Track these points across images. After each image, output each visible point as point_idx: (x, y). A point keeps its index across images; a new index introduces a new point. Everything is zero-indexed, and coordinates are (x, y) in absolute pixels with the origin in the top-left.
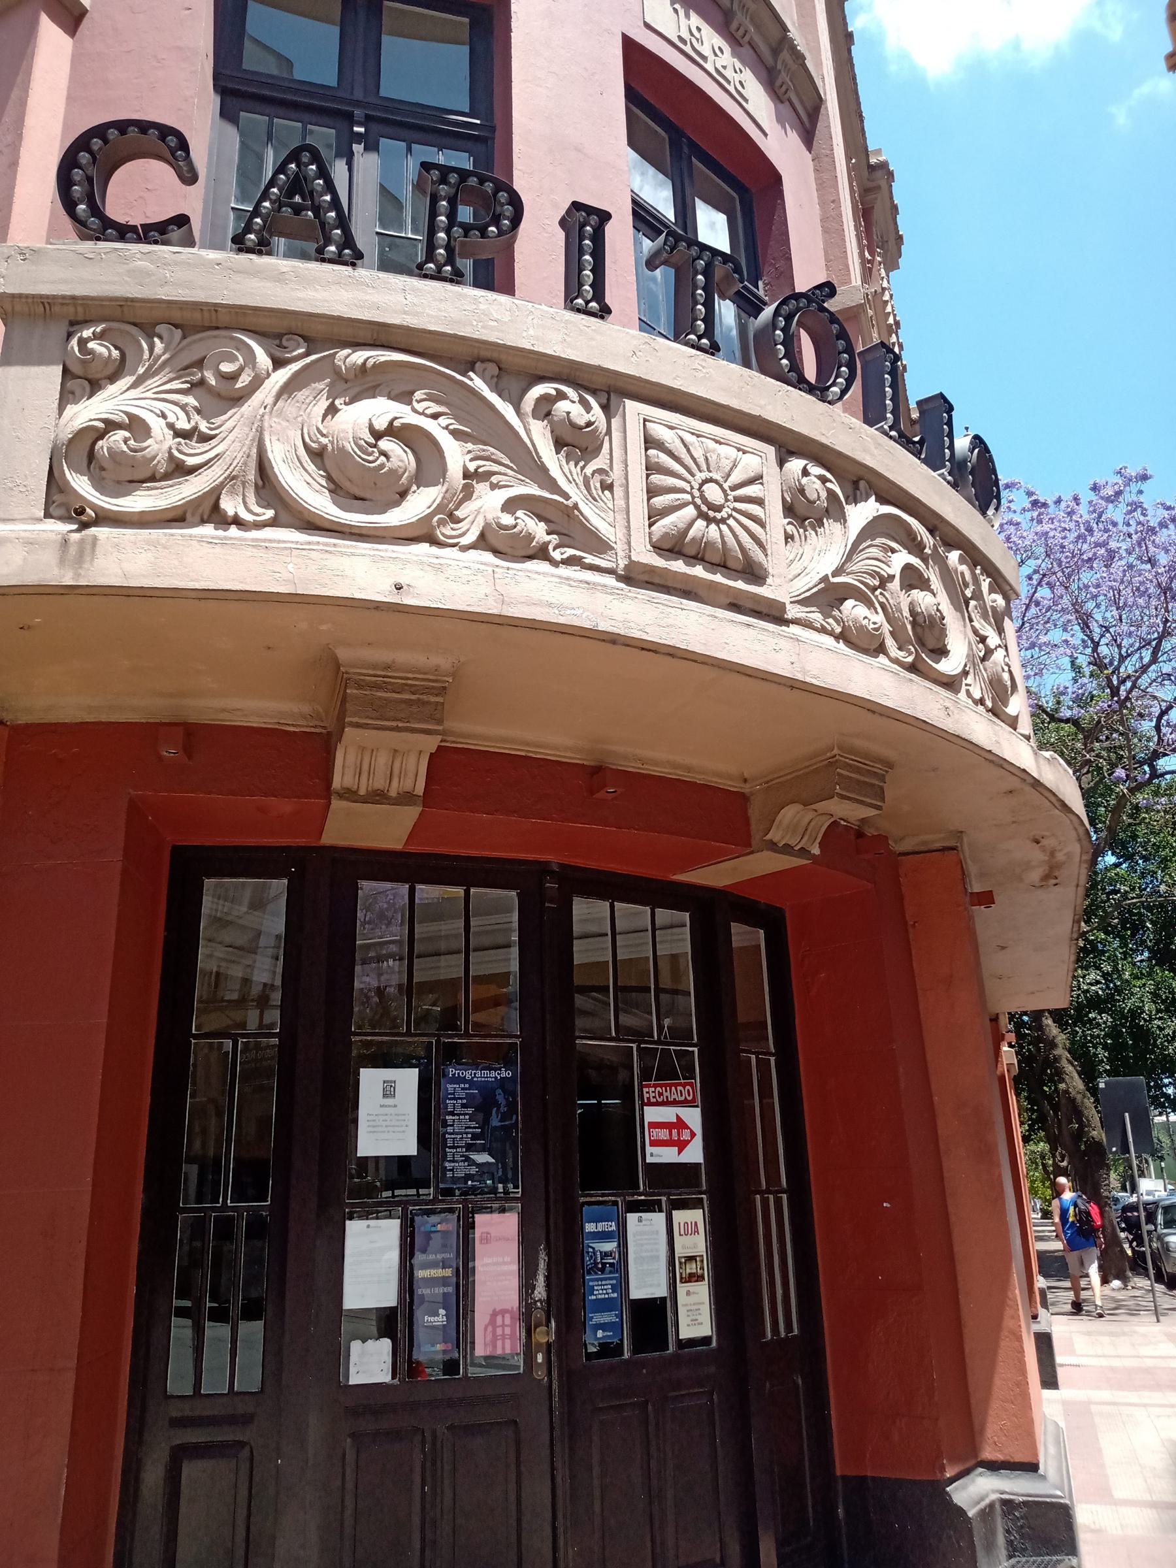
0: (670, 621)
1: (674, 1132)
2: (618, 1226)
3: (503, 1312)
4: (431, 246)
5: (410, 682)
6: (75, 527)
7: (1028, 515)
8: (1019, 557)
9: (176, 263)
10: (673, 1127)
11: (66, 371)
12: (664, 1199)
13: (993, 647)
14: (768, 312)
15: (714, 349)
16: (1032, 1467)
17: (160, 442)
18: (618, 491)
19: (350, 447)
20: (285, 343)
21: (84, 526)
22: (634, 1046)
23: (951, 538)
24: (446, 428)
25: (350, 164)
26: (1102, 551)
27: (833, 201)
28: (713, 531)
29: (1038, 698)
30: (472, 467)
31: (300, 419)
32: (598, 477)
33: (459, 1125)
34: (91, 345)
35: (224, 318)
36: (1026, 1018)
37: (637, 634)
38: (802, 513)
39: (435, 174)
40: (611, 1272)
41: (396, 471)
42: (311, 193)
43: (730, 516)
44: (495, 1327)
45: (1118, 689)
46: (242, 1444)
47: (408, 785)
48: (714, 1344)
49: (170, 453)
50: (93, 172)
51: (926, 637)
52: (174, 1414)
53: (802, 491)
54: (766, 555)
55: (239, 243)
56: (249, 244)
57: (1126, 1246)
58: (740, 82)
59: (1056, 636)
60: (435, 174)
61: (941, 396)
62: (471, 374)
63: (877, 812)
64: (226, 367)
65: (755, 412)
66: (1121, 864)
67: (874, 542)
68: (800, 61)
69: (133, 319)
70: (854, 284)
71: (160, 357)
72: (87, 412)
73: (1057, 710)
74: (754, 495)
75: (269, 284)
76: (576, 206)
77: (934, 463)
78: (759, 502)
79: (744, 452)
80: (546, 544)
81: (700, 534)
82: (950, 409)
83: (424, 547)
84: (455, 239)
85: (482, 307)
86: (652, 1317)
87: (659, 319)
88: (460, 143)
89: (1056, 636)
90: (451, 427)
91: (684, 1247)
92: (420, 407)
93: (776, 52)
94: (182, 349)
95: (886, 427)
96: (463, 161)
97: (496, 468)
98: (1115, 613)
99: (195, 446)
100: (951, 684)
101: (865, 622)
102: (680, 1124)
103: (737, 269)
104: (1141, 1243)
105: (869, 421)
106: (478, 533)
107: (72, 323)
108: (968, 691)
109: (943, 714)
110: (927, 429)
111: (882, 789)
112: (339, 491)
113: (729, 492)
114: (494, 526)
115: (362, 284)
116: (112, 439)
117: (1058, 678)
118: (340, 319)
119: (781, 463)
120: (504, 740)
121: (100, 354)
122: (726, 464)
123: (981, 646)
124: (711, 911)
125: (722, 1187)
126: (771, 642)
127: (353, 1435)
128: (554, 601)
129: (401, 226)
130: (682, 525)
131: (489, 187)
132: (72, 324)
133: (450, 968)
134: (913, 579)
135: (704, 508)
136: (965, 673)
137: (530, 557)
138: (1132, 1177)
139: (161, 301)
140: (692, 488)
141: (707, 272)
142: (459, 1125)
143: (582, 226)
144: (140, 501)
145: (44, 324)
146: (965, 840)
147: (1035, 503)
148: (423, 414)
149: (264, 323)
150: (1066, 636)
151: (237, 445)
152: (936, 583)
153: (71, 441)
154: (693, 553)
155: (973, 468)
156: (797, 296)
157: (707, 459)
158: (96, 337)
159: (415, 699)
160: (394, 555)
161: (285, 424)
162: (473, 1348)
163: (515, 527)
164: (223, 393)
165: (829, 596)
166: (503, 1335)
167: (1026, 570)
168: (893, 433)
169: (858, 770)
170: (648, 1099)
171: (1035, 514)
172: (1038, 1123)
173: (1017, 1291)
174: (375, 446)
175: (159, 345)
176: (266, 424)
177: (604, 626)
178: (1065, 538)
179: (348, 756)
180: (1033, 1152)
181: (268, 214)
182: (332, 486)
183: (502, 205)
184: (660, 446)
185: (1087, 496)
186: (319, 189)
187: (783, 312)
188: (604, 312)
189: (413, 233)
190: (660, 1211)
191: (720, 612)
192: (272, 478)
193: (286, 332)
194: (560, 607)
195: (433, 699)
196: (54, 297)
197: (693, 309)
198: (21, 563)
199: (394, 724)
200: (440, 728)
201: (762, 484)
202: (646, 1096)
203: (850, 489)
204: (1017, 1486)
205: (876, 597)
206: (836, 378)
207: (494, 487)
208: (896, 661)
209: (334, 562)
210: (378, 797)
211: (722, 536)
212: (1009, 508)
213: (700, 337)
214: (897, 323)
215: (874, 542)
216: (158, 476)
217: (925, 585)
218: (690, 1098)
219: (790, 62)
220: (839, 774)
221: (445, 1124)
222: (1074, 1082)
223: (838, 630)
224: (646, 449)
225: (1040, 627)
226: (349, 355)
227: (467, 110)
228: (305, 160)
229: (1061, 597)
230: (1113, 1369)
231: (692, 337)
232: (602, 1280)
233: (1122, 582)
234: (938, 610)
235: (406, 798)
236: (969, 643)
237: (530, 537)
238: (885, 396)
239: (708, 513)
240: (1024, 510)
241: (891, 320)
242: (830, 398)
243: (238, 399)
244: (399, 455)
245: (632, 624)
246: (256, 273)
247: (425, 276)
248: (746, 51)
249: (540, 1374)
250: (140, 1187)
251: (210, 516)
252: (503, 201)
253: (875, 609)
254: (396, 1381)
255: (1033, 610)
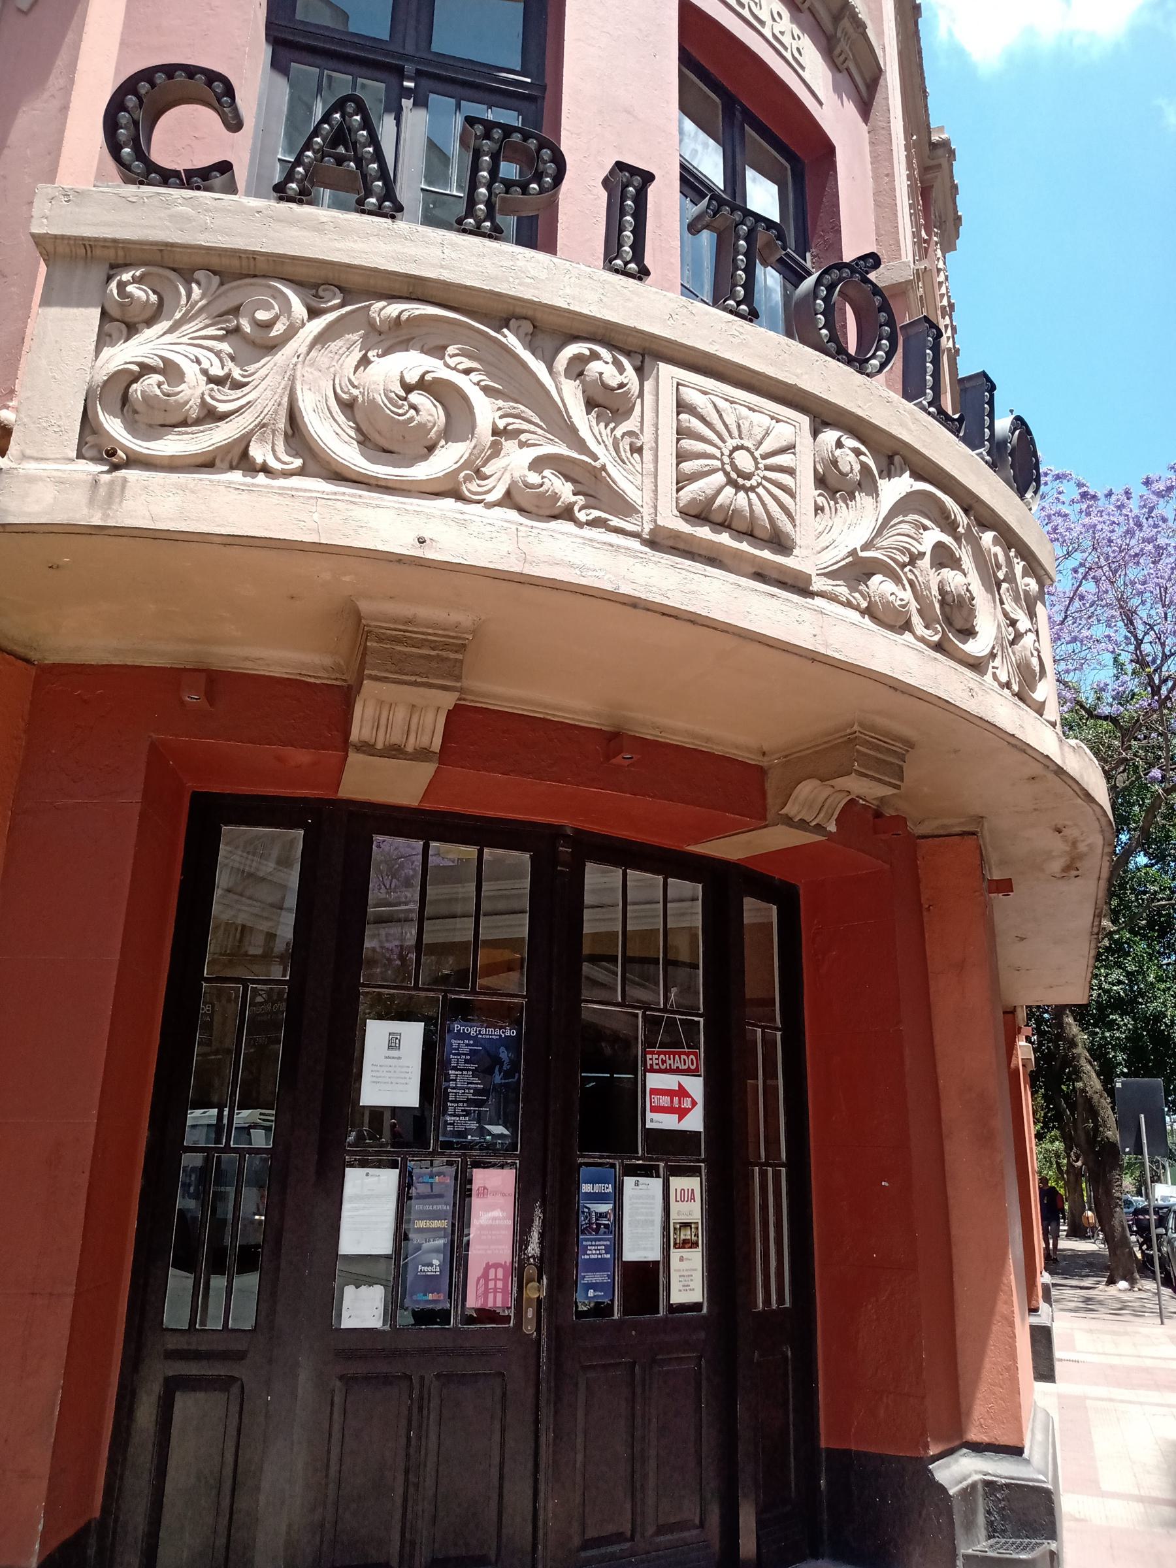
0: (693, 587)
1: (676, 1099)
2: (615, 1188)
3: (496, 1266)
4: (471, 202)
5: (430, 637)
6: (106, 468)
7: (1077, 507)
8: (1065, 549)
9: (217, 210)
10: (674, 1096)
11: (104, 314)
12: (662, 1164)
13: (1022, 631)
14: (810, 282)
15: (752, 316)
16: (1016, 1451)
17: (193, 389)
18: (647, 454)
19: (380, 399)
20: (321, 293)
21: (116, 467)
22: (640, 1012)
23: (985, 518)
24: (478, 384)
25: (398, 120)
26: (1150, 547)
27: (887, 175)
28: (741, 499)
29: (1078, 691)
30: (501, 424)
31: (332, 370)
32: (627, 440)
33: (462, 1082)
34: (130, 288)
35: (262, 266)
36: (1046, 1016)
37: (659, 599)
38: (832, 484)
39: (479, 129)
40: (605, 1233)
41: (425, 425)
42: (354, 144)
43: (759, 484)
44: (487, 1280)
45: (1159, 688)
46: (233, 1379)
47: (424, 741)
48: (705, 1310)
49: (202, 398)
50: (140, 115)
51: (955, 617)
52: (170, 1347)
53: (835, 463)
54: (795, 526)
55: (280, 192)
56: (290, 193)
57: (1136, 1249)
58: (798, 49)
59: (1099, 631)
60: (479, 129)
61: (984, 374)
62: (505, 330)
63: (896, 791)
64: (262, 315)
65: (791, 380)
66: (1153, 865)
67: (906, 519)
68: (861, 30)
69: (172, 264)
70: (904, 259)
71: (197, 303)
72: (124, 354)
73: (1095, 707)
74: (785, 464)
75: (306, 234)
76: (620, 166)
77: (972, 442)
78: (791, 471)
79: (778, 421)
80: (573, 504)
81: (728, 502)
82: (992, 388)
83: (449, 502)
84: (496, 195)
85: (519, 263)
86: (645, 1280)
87: (702, 286)
88: (509, 101)
89: (1099, 631)
90: (482, 383)
91: (679, 1213)
92: (452, 362)
93: (836, 19)
94: (220, 296)
95: (925, 403)
96: (511, 118)
97: (532, 428)
98: (1161, 610)
99: (227, 393)
100: (977, 665)
101: (892, 598)
102: (682, 1092)
103: (781, 236)
104: (1150, 1247)
105: (908, 396)
106: (503, 491)
107: (112, 267)
108: (994, 674)
109: (967, 695)
110: (969, 407)
111: (901, 768)
112: (367, 443)
113: (760, 460)
114: (521, 484)
115: (400, 236)
116: (146, 382)
117: (1099, 676)
118: (376, 271)
119: (815, 433)
120: (522, 701)
121: (139, 298)
122: (758, 433)
123: (1011, 629)
124: (724, 885)
125: (720, 1154)
126: (795, 612)
127: (341, 1378)
128: (576, 561)
129: (446, 183)
130: (710, 492)
131: (533, 143)
132: (112, 267)
133: (462, 931)
134: (943, 558)
135: (734, 475)
136: (993, 656)
137: (555, 517)
138: (1145, 1182)
139: (201, 247)
140: (722, 454)
141: (749, 238)
142: (462, 1082)
143: (625, 186)
144: (171, 445)
145: (84, 264)
146: (986, 825)
147: (1084, 495)
148: (455, 369)
149: (301, 272)
150: (1111, 632)
151: (269, 393)
152: (967, 562)
153: (106, 383)
154: (720, 520)
155: (1013, 449)
156: (841, 266)
157: (739, 426)
158: (135, 280)
159: (435, 655)
160: (419, 509)
161: (317, 374)
162: (464, 1299)
163: (541, 486)
164: (258, 341)
165: (857, 570)
166: (495, 1288)
167: (1072, 563)
168: (932, 409)
169: (877, 748)
170: (651, 1065)
171: (1084, 506)
172: (1050, 1121)
173: (1012, 1277)
174: (405, 399)
175: (196, 291)
176: (298, 374)
177: (625, 589)
178: (1113, 531)
179: (366, 710)
180: (1047, 1150)
181: (310, 164)
182: (361, 438)
183: (545, 162)
184: (692, 410)
185: (1139, 490)
186: (362, 140)
187: (825, 281)
188: (643, 273)
189: (458, 190)
190: (658, 1176)
191: (744, 581)
192: (302, 427)
193: (322, 282)
194: (582, 568)
195: (452, 656)
196: (96, 240)
197: (733, 276)
198: (52, 501)
199: (413, 678)
200: (459, 685)
201: (794, 454)
202: (649, 1062)
203: (885, 461)
204: (1001, 1469)
205: (905, 574)
206: (876, 350)
207: (522, 445)
208: (922, 640)
209: (360, 513)
210: (395, 751)
211: (750, 505)
212: (1058, 499)
213: (739, 303)
214: (952, 306)
215: (906, 519)
216: (189, 421)
217: (956, 564)
218: (693, 1067)
219: (851, 30)
220: (858, 751)
221: (448, 1080)
222: (1092, 1082)
223: (864, 605)
224: (678, 414)
225: (1084, 622)
226: (384, 307)
227: (518, 69)
228: (350, 110)
229: (1106, 592)
230: (1112, 1367)
231: (731, 302)
232: (596, 1240)
233: (1170, 579)
234: (968, 590)
235: (422, 754)
236: (999, 625)
237: (555, 497)
238: (926, 372)
239: (738, 480)
240: (1073, 501)
241: (945, 302)
242: (869, 371)
243: (272, 347)
244: (429, 410)
245: (654, 589)
246: (295, 222)
247: (464, 231)
248: (806, 16)
249: (529, 1329)
250: (146, 1124)
251: (238, 464)
252: (546, 158)
253: (903, 586)
254: (387, 1328)
255: (1077, 604)
